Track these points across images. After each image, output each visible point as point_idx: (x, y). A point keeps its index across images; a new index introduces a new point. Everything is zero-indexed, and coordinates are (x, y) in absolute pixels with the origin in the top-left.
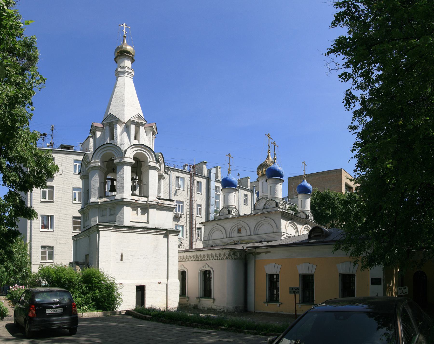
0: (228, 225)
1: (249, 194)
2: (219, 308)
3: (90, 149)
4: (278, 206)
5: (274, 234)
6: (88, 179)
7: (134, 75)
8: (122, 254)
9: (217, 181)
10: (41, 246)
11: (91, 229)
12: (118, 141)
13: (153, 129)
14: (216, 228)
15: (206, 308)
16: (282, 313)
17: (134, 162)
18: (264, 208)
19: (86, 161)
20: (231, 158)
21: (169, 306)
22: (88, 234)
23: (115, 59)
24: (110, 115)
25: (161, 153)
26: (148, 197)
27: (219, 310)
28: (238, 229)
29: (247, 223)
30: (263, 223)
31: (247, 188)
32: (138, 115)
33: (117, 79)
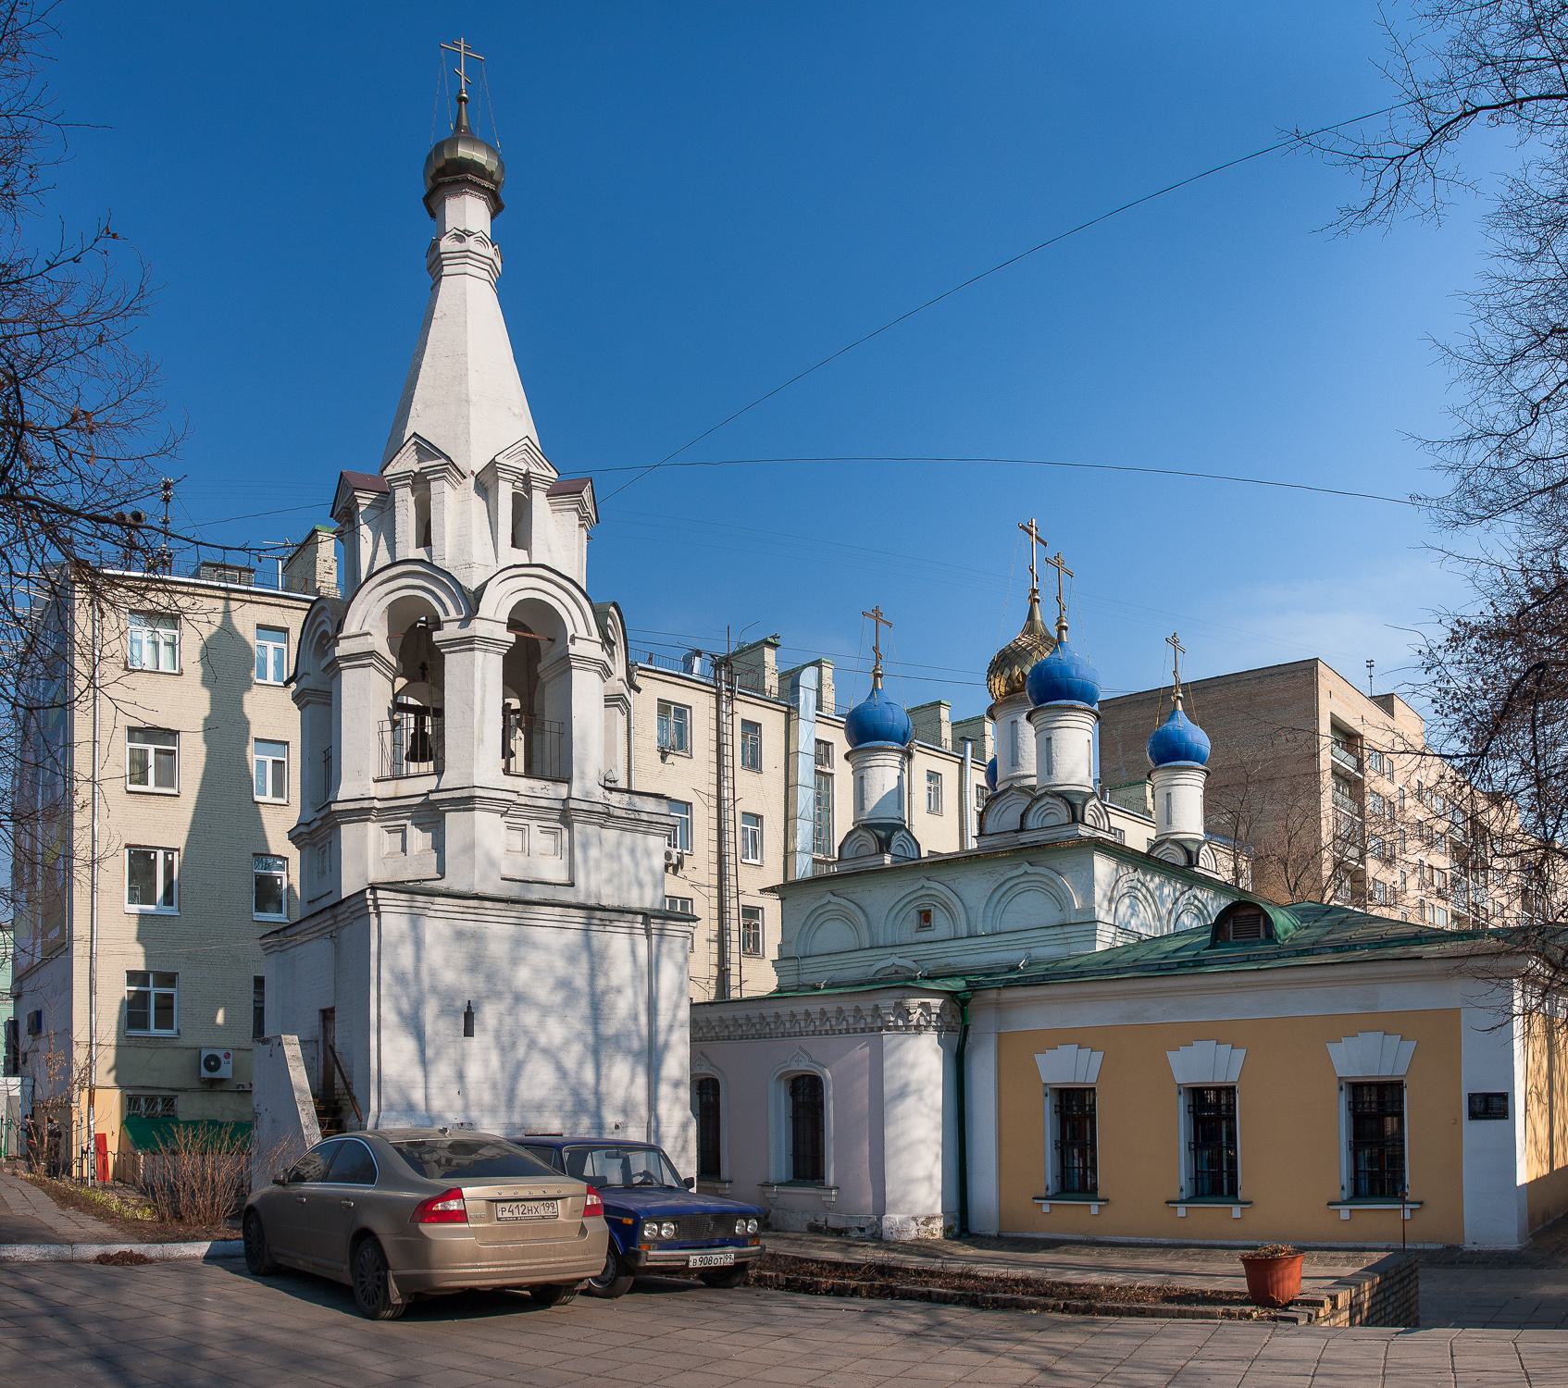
0: (881, 899)
1: (949, 770)
3: (318, 585)
4: (1079, 818)
5: (1067, 929)
6: (330, 705)
7: (500, 269)
8: (469, 1007)
9: (821, 719)
10: (41, 1011)
11: (342, 908)
12: (447, 550)
13: (582, 503)
14: (830, 907)
17: (512, 637)
18: (1022, 829)
19: (316, 631)
20: (880, 624)
21: (784, 1180)
22: (332, 928)
23: (427, 200)
24: (416, 442)
25: (615, 605)
26: (693, 1178)
28: (920, 912)
29: (954, 888)
30: (1022, 886)
31: (940, 746)
32: (526, 441)
33: (435, 285)
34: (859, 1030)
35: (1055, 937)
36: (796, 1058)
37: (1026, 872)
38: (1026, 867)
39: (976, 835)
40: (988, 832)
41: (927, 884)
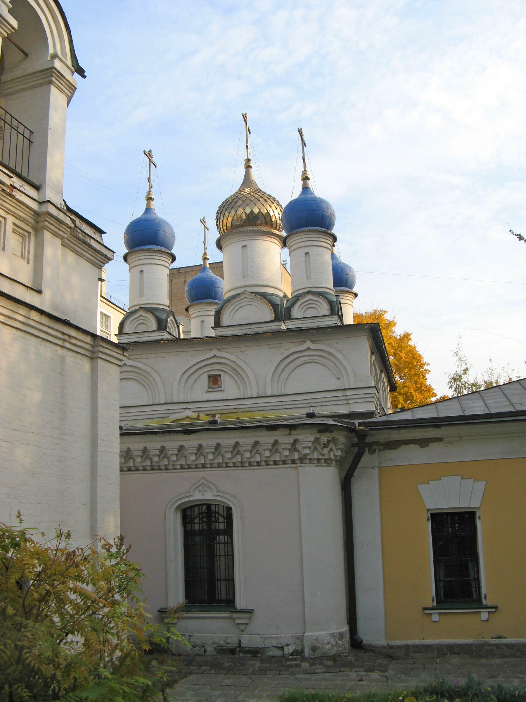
2: (275, 643)
5: (348, 393)
15: (209, 649)
16: (503, 641)
27: (279, 653)
28: (210, 377)
34: (272, 463)
35: (337, 399)
36: (200, 489)
37: (308, 348)
38: (309, 344)
39: (117, 333)
40: (224, 324)
41: (219, 354)
